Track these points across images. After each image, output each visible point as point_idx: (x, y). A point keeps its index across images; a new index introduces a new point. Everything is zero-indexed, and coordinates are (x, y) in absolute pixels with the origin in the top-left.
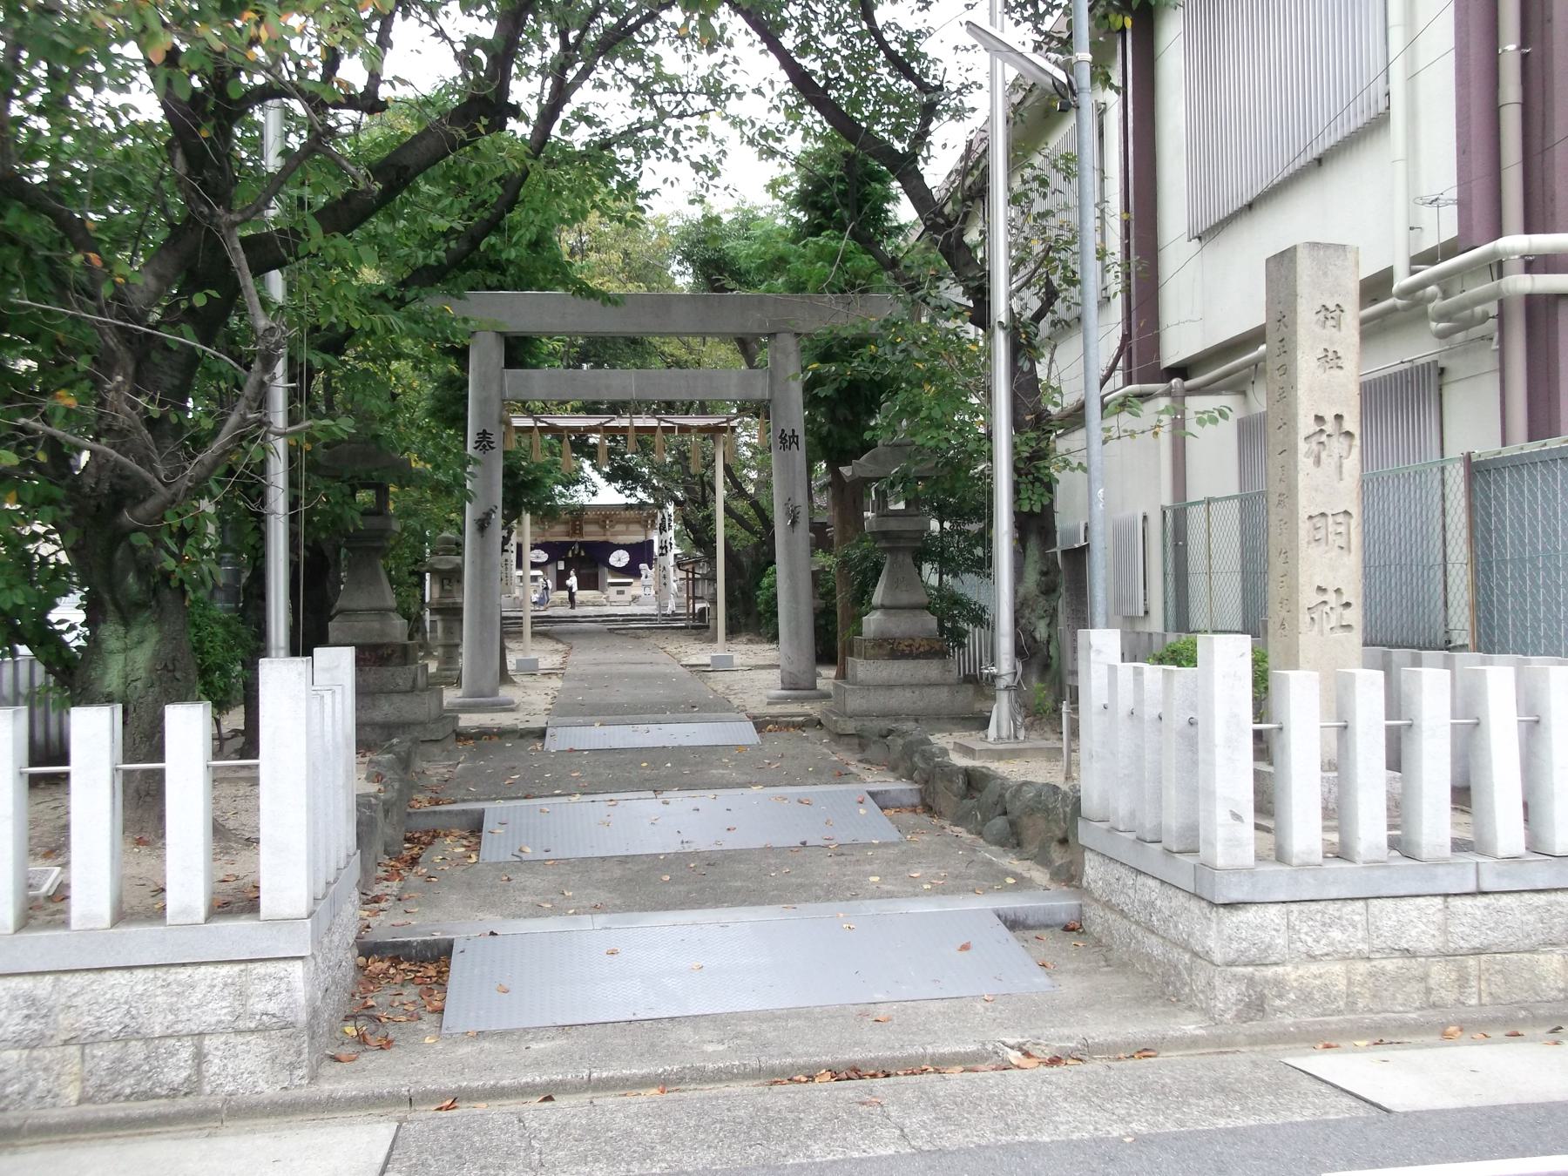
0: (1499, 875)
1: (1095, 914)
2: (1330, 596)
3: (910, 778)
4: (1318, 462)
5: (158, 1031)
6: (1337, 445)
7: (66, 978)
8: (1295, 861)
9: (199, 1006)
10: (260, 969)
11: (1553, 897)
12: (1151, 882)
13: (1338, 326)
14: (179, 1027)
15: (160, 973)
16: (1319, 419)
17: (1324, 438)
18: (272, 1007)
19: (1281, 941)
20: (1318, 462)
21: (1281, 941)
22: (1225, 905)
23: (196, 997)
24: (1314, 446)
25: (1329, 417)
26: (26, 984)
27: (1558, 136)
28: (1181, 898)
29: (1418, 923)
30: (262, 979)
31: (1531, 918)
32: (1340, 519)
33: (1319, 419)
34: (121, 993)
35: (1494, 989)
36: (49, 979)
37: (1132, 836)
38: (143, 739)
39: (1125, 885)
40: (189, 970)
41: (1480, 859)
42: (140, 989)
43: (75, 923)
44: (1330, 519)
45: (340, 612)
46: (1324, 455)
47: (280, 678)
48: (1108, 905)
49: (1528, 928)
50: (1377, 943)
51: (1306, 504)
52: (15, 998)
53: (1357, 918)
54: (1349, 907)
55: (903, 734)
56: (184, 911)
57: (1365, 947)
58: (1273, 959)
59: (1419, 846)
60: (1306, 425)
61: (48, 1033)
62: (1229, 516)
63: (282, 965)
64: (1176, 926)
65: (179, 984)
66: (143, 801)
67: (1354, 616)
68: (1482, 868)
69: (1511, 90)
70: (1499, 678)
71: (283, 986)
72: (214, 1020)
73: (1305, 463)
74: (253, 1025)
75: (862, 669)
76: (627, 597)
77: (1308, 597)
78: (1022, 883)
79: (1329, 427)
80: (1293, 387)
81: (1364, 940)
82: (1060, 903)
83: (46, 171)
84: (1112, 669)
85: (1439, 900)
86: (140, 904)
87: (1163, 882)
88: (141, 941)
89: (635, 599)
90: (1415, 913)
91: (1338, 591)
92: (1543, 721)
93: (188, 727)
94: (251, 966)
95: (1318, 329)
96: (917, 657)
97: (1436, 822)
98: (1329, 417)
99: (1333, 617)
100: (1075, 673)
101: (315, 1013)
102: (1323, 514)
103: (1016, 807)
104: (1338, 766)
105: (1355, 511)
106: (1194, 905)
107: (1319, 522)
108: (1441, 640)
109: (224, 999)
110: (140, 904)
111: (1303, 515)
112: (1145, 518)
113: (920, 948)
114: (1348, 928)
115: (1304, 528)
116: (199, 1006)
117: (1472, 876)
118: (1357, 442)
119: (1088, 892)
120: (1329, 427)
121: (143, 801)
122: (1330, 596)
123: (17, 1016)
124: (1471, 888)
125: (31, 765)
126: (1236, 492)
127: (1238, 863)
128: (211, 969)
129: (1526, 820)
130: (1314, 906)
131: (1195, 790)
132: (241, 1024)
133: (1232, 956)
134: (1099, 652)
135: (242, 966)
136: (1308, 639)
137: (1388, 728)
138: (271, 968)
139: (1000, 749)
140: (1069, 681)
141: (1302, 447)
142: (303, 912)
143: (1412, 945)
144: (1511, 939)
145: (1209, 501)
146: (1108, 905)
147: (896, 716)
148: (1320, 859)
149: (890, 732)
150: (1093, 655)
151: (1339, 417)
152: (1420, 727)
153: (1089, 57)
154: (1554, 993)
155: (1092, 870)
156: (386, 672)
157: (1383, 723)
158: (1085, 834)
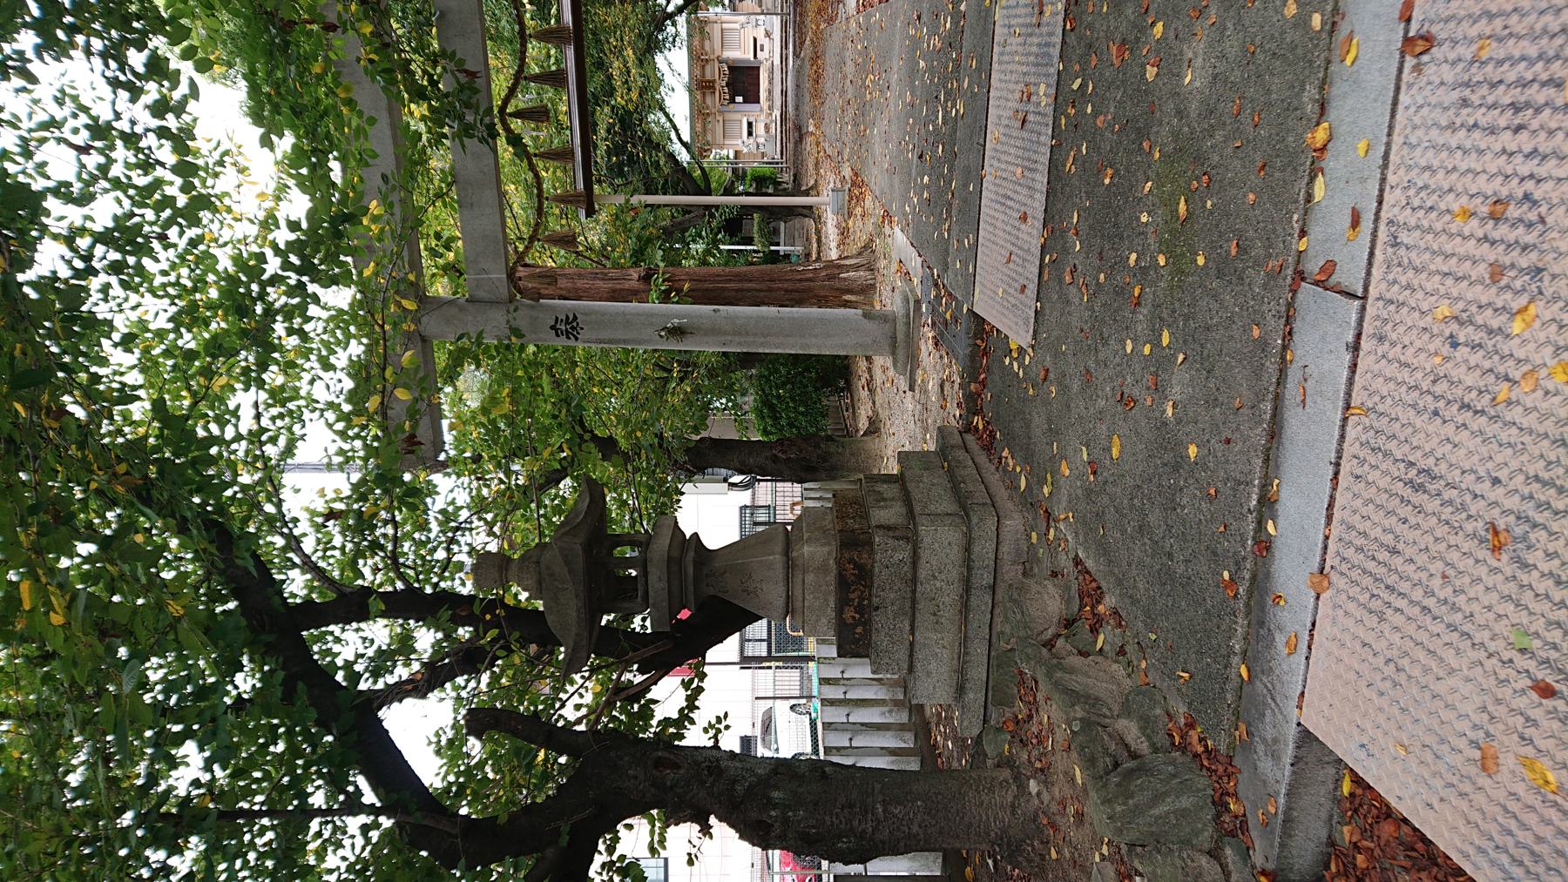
89: (768, 34)
156: (881, 575)
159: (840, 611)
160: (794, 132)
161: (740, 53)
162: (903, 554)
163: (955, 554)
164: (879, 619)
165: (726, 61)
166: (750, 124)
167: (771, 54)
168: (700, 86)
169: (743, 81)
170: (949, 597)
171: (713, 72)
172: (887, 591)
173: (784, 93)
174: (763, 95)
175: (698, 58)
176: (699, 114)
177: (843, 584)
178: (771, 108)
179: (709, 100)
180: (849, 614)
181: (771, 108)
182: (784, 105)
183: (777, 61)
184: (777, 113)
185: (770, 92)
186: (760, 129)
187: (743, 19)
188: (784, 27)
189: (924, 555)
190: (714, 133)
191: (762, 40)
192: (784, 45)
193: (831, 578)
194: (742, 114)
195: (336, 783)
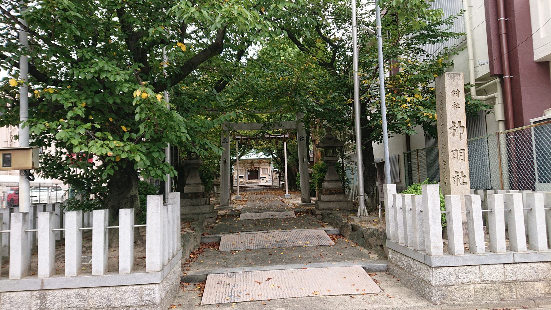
0: (521, 257)
1: (392, 267)
2: (460, 174)
3: (336, 227)
4: (454, 135)
5: (117, 305)
6: (459, 130)
7: (91, 289)
8: (456, 254)
9: (128, 298)
10: (146, 287)
11: (538, 264)
12: (410, 259)
13: (458, 96)
14: (122, 304)
15: (117, 288)
16: (453, 122)
17: (455, 128)
18: (149, 298)
19: (453, 278)
20: (454, 135)
21: (453, 278)
22: (434, 267)
23: (127, 295)
24: (452, 131)
25: (457, 122)
26: (80, 291)
27: (518, 42)
28: (420, 265)
29: (496, 273)
30: (146, 290)
31: (531, 271)
32: (462, 151)
33: (453, 122)
34: (106, 294)
35: (521, 294)
36: (86, 290)
37: (412, 249)
38: (114, 219)
39: (401, 260)
40: (126, 287)
41: (514, 253)
42: (111, 293)
43: (93, 273)
44: (458, 152)
45: (187, 184)
46: (455, 133)
47: (153, 202)
48: (396, 265)
49: (531, 274)
50: (484, 279)
51: (451, 148)
52: (77, 295)
53: (476, 271)
54: (474, 268)
55: (333, 214)
56: (124, 270)
57: (479, 280)
58: (451, 284)
59: (496, 249)
60: (449, 124)
61: (86, 305)
62: (423, 154)
63: (152, 285)
64: (419, 273)
65: (122, 291)
66: (113, 236)
67: (467, 180)
68: (515, 255)
69: (503, 31)
70: (517, 196)
71: (152, 292)
72: (132, 302)
73: (450, 135)
74: (143, 304)
75: (324, 197)
76: (265, 181)
77: (452, 174)
78: (368, 257)
79: (457, 125)
80: (445, 114)
81: (479, 278)
82: (383, 265)
83: (315, 201)
84: (394, 195)
85: (502, 265)
86: (112, 267)
87: (414, 259)
88: (112, 279)
89: (267, 181)
90: (495, 269)
91: (462, 172)
92: (533, 210)
93: (126, 216)
94: (143, 286)
95: (452, 97)
96: (337, 194)
97: (501, 242)
98: (457, 122)
99: (461, 180)
100: (383, 197)
101: (162, 300)
102: (456, 150)
103: (366, 235)
104: (467, 226)
105: (466, 149)
106: (425, 267)
107: (455, 152)
108: (490, 187)
109: (135, 296)
110: (112, 267)
111: (450, 150)
112: (399, 156)
113: (342, 279)
114: (473, 274)
115: (450, 154)
116: (128, 298)
117: (512, 258)
118: (465, 129)
119: (391, 261)
120: (457, 125)
121: (113, 236)
122: (460, 174)
123: (77, 300)
124: (512, 262)
125: (135, 224)
126: (424, 147)
127: (438, 254)
128: (132, 287)
129: (507, 238)
130: (463, 268)
131: (426, 233)
132: (140, 304)
133: (438, 283)
134: (390, 191)
135: (140, 286)
136: (453, 187)
137: (483, 212)
138: (149, 286)
139: (362, 220)
140: (380, 199)
141: (449, 131)
142: (159, 270)
143: (495, 280)
144: (525, 278)
145: (417, 150)
146: (396, 265)
147: (332, 210)
148: (463, 253)
149: (330, 214)
150: (388, 191)
151: (459, 122)
152: (495, 212)
153: (381, 27)
154: (540, 295)
155: (390, 254)
156: (198, 200)
157: (504, 210)
158: (388, 244)
159: (190, 193)
160: (244, 189)
161: (262, 174)
162: (202, 203)
163: (204, 212)
164: (190, 200)
165: (259, 169)
166: (242, 177)
167: (262, 182)
168: (252, 162)
169: (254, 175)
170: (195, 211)
171: (256, 165)
172: (195, 201)
173: (252, 187)
174: (250, 181)
175: (259, 161)
176: (245, 161)
177: (196, 193)
178: (247, 183)
179: (248, 164)
180: (190, 195)
181: (247, 183)
182: (249, 187)
183: (260, 184)
184: (246, 185)
185: (251, 183)
186: (241, 180)
187: (271, 174)
188: (270, 186)
189: (204, 206)
190: (265, 165)
191: (266, 180)
192: (265, 186)
193: (196, 191)
194: (245, 174)
195: (123, 59)
